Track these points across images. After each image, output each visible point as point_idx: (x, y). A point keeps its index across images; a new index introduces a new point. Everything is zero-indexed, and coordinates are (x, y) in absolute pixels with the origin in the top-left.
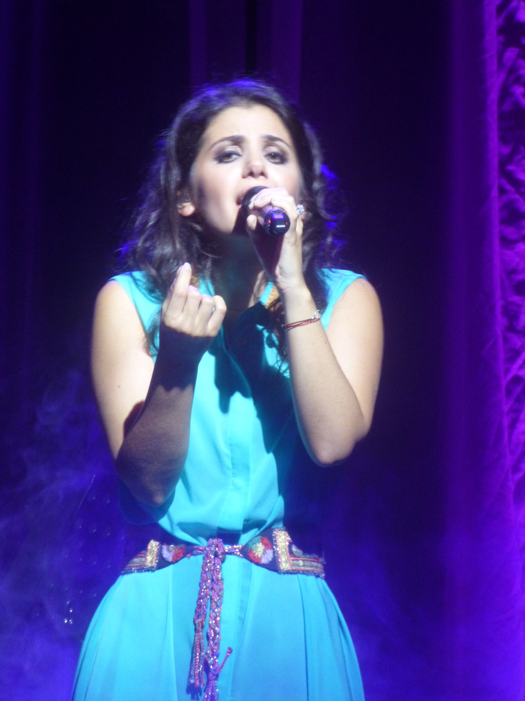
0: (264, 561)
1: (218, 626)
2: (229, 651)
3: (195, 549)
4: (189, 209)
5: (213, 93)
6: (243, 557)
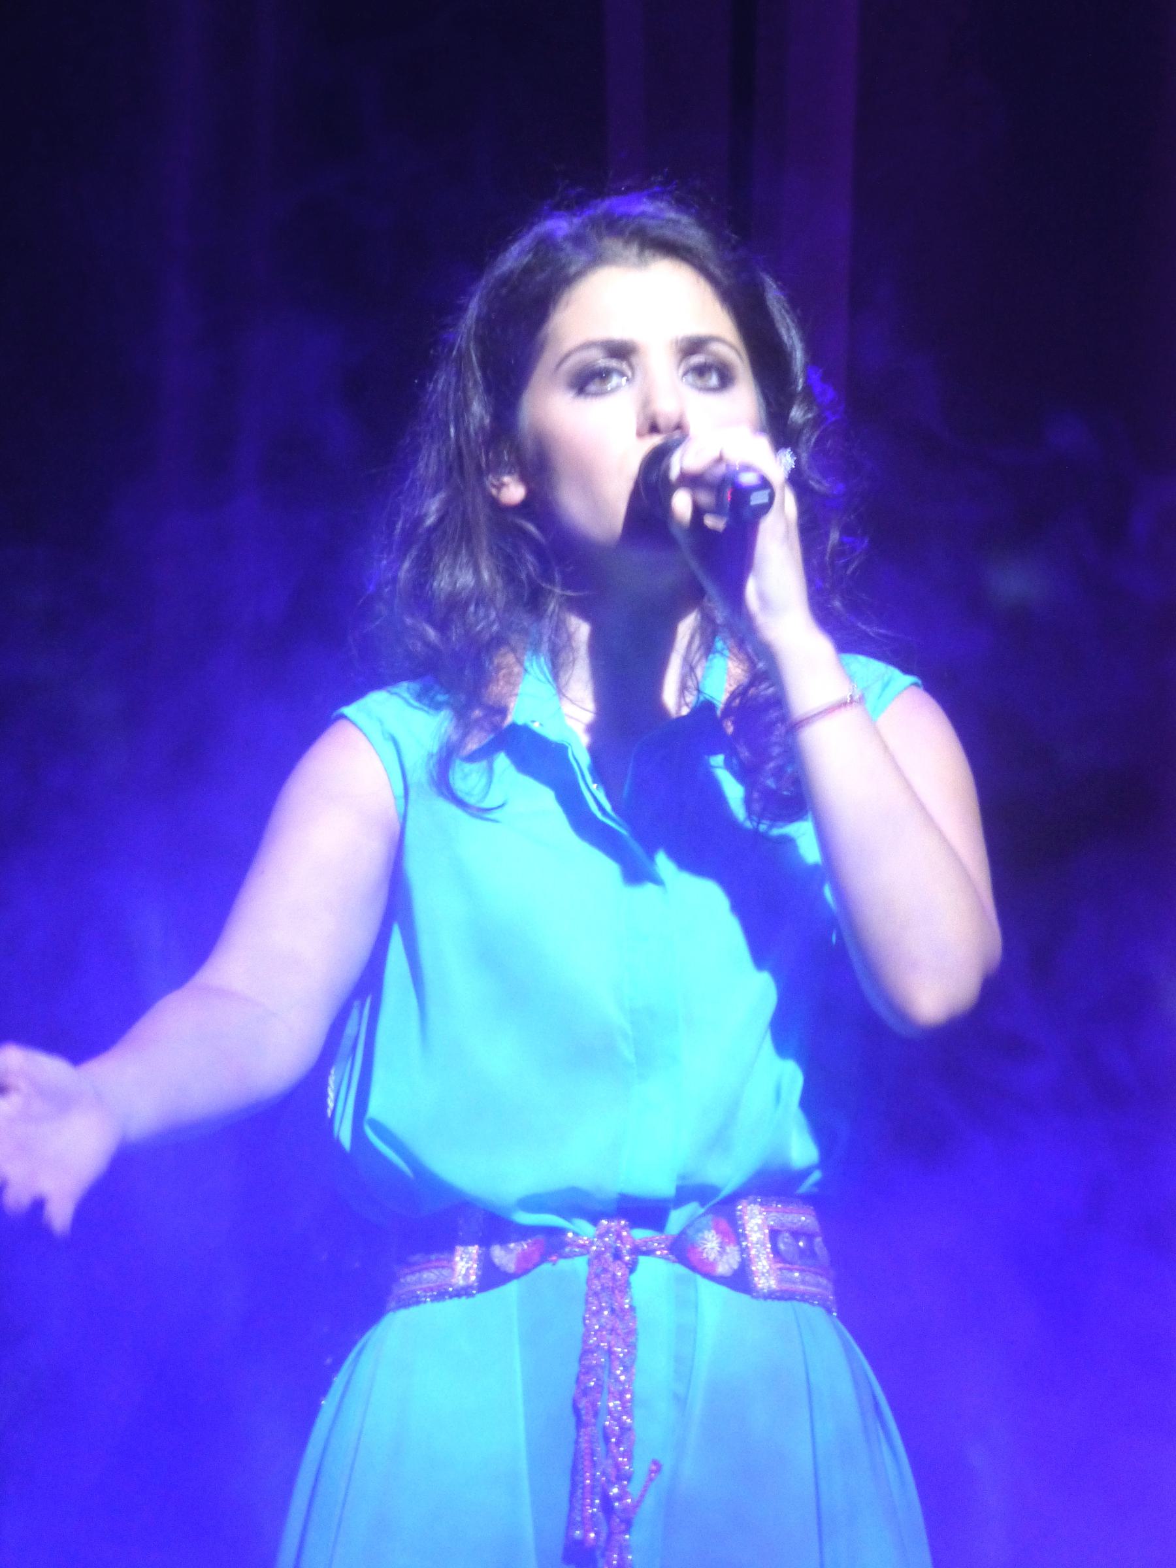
0: (722, 1269)
1: (630, 1415)
2: (654, 1468)
3: (568, 1244)
4: (514, 492)
5: (561, 226)
6: (674, 1262)
